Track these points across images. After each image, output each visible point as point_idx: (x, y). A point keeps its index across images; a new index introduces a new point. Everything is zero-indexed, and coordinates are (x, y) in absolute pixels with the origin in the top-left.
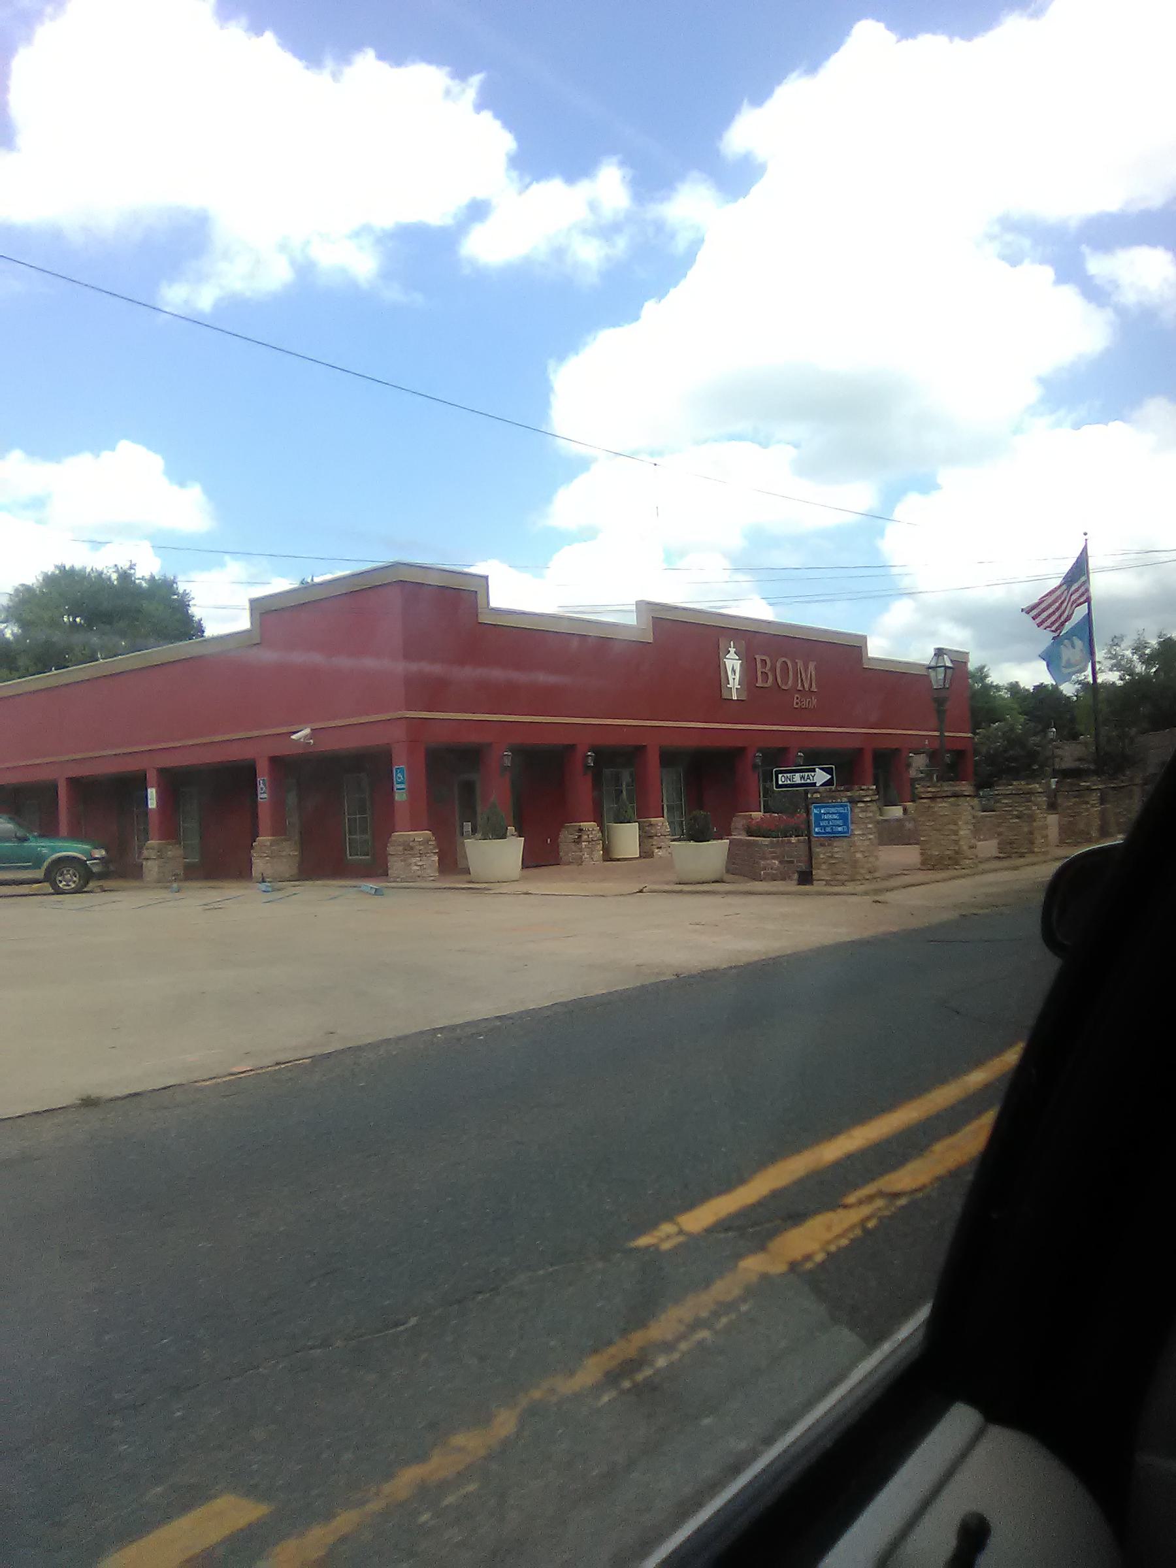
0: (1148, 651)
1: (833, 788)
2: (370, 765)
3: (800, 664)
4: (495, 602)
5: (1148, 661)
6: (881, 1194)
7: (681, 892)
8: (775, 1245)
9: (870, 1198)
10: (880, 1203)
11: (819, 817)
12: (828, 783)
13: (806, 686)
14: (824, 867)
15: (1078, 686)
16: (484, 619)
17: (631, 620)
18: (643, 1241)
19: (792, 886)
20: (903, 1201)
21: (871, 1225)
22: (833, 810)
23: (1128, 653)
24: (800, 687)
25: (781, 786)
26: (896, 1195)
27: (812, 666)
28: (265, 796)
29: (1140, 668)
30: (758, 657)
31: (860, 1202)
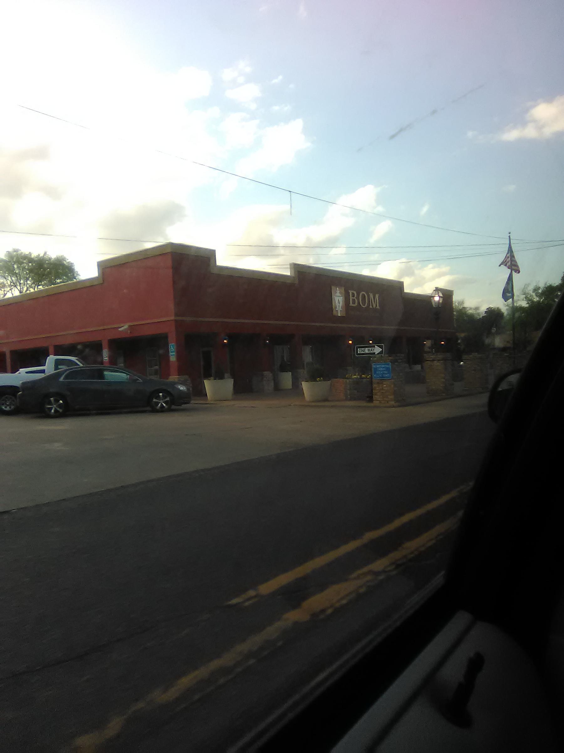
0: (540, 291)
1: (383, 355)
2: (157, 342)
3: (371, 296)
4: (405, 291)
5: (540, 295)
6: (370, 572)
7: (318, 406)
8: (306, 604)
9: (365, 574)
10: (369, 578)
11: (376, 369)
12: (381, 353)
13: (374, 306)
14: (379, 394)
15: (507, 307)
16: (215, 271)
17: (287, 272)
18: (234, 601)
19: (364, 404)
20: (381, 577)
21: (362, 590)
22: (383, 366)
23: (531, 292)
24: (371, 307)
25: (360, 354)
26: (377, 574)
27: (377, 296)
28: (106, 358)
29: (536, 299)
30: (351, 292)
31: (358, 578)
